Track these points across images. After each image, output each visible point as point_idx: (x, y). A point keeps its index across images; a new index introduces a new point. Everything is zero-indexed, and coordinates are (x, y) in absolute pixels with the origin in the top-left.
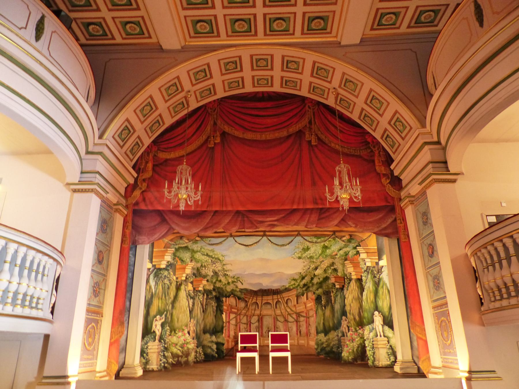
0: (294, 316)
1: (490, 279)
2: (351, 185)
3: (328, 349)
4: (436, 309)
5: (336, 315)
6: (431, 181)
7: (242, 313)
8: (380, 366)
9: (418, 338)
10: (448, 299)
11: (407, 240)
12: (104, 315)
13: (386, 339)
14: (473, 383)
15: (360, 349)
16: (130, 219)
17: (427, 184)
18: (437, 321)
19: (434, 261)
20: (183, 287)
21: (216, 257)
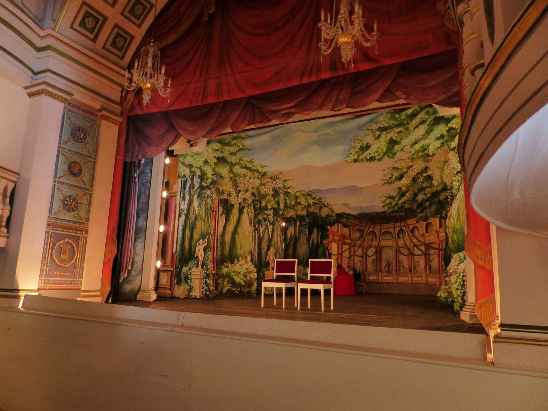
0: (422, 248)
7: (357, 245)
12: (89, 233)
16: (124, 127)
20: (245, 210)
21: (255, 169)
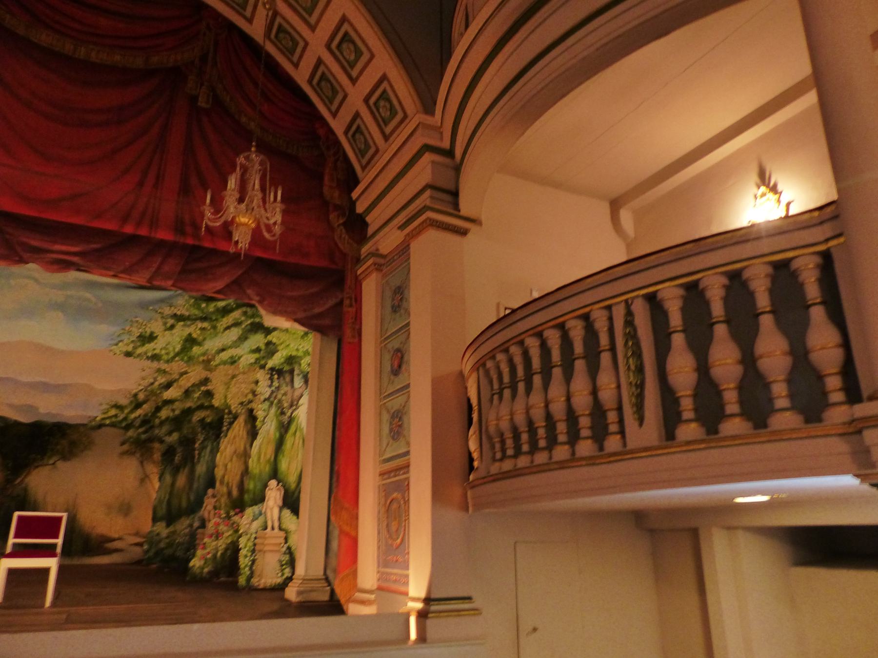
1: (502, 415)
2: (264, 200)
3: (169, 552)
4: (386, 476)
5: (195, 486)
6: (423, 222)
8: (261, 586)
9: (342, 532)
10: (413, 458)
11: (356, 340)
13: (282, 534)
14: (429, 622)
15: (229, 552)
17: (416, 228)
18: (383, 499)
19: (399, 384)
